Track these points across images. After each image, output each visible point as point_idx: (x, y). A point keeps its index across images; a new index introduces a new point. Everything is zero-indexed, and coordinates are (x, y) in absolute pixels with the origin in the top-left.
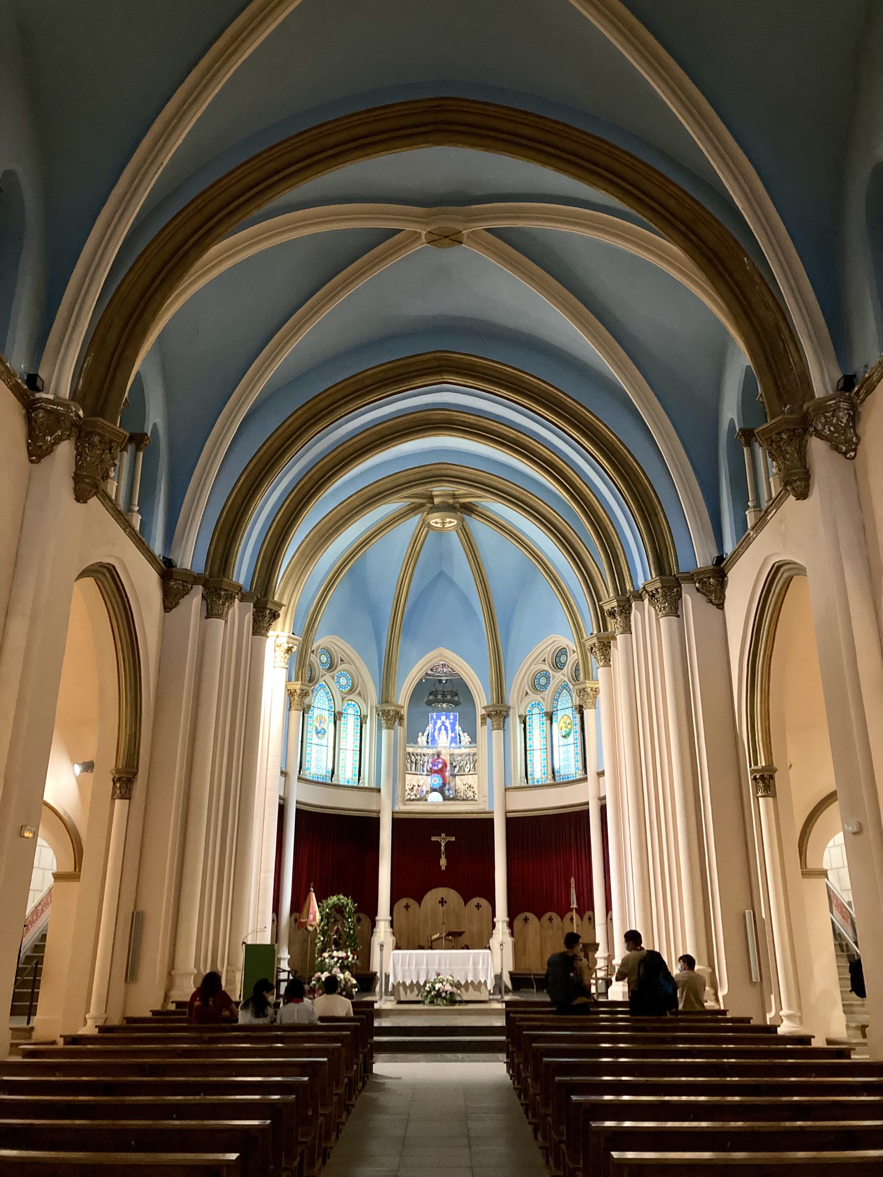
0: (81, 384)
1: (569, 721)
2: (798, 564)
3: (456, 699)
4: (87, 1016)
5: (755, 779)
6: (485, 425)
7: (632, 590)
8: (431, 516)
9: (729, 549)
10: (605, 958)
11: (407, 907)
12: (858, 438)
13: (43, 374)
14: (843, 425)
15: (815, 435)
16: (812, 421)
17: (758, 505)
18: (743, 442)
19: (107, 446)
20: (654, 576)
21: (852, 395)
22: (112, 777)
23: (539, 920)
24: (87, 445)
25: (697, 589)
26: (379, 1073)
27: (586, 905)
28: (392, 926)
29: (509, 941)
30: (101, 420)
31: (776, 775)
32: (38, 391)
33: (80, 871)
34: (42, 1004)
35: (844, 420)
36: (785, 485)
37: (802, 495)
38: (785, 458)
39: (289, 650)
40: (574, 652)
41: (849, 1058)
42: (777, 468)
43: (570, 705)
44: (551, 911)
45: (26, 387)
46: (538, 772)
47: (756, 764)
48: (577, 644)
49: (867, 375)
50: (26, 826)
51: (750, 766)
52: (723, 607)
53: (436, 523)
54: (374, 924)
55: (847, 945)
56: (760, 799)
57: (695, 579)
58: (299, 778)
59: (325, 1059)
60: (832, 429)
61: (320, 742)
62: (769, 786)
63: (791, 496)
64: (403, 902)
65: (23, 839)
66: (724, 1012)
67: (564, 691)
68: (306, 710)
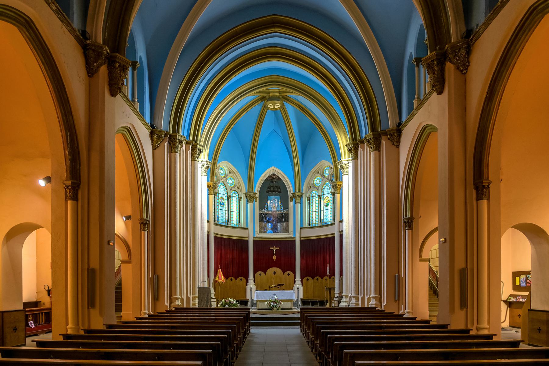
0: (106, 36)
1: (328, 199)
2: (435, 126)
3: (280, 190)
4: (141, 312)
5: (405, 222)
6: (295, 55)
7: (360, 139)
8: (268, 102)
9: (404, 119)
10: (338, 294)
11: (260, 275)
12: (469, 63)
13: (88, 30)
14: (463, 56)
15: (449, 62)
16: (449, 54)
17: (419, 98)
18: (416, 65)
19: (122, 68)
20: (370, 132)
21: (469, 40)
22: (139, 222)
23: (313, 279)
24: (113, 68)
25: (389, 139)
26: (252, 332)
27: (333, 274)
28: (254, 282)
29: (301, 288)
30: (117, 54)
31: (414, 221)
32: (88, 39)
33: (131, 259)
34: (123, 308)
35: (464, 54)
36: (433, 88)
37: (440, 92)
38: (434, 73)
39: (207, 167)
40: (332, 168)
41: (429, 323)
42: (430, 79)
43: (329, 192)
44: (318, 276)
45: (82, 37)
46: (314, 221)
47: (406, 216)
48: (334, 165)
49: (477, 30)
50: (110, 241)
51: (404, 217)
52: (399, 147)
53: (271, 106)
54: (247, 281)
55: (433, 287)
56: (406, 231)
57: (388, 133)
58: (215, 224)
59: (211, 351)
60: (458, 58)
61: (221, 208)
62: (411, 225)
63: (435, 93)
64: (259, 273)
65: (110, 246)
66: (384, 311)
67: (327, 186)
68: (215, 194)
